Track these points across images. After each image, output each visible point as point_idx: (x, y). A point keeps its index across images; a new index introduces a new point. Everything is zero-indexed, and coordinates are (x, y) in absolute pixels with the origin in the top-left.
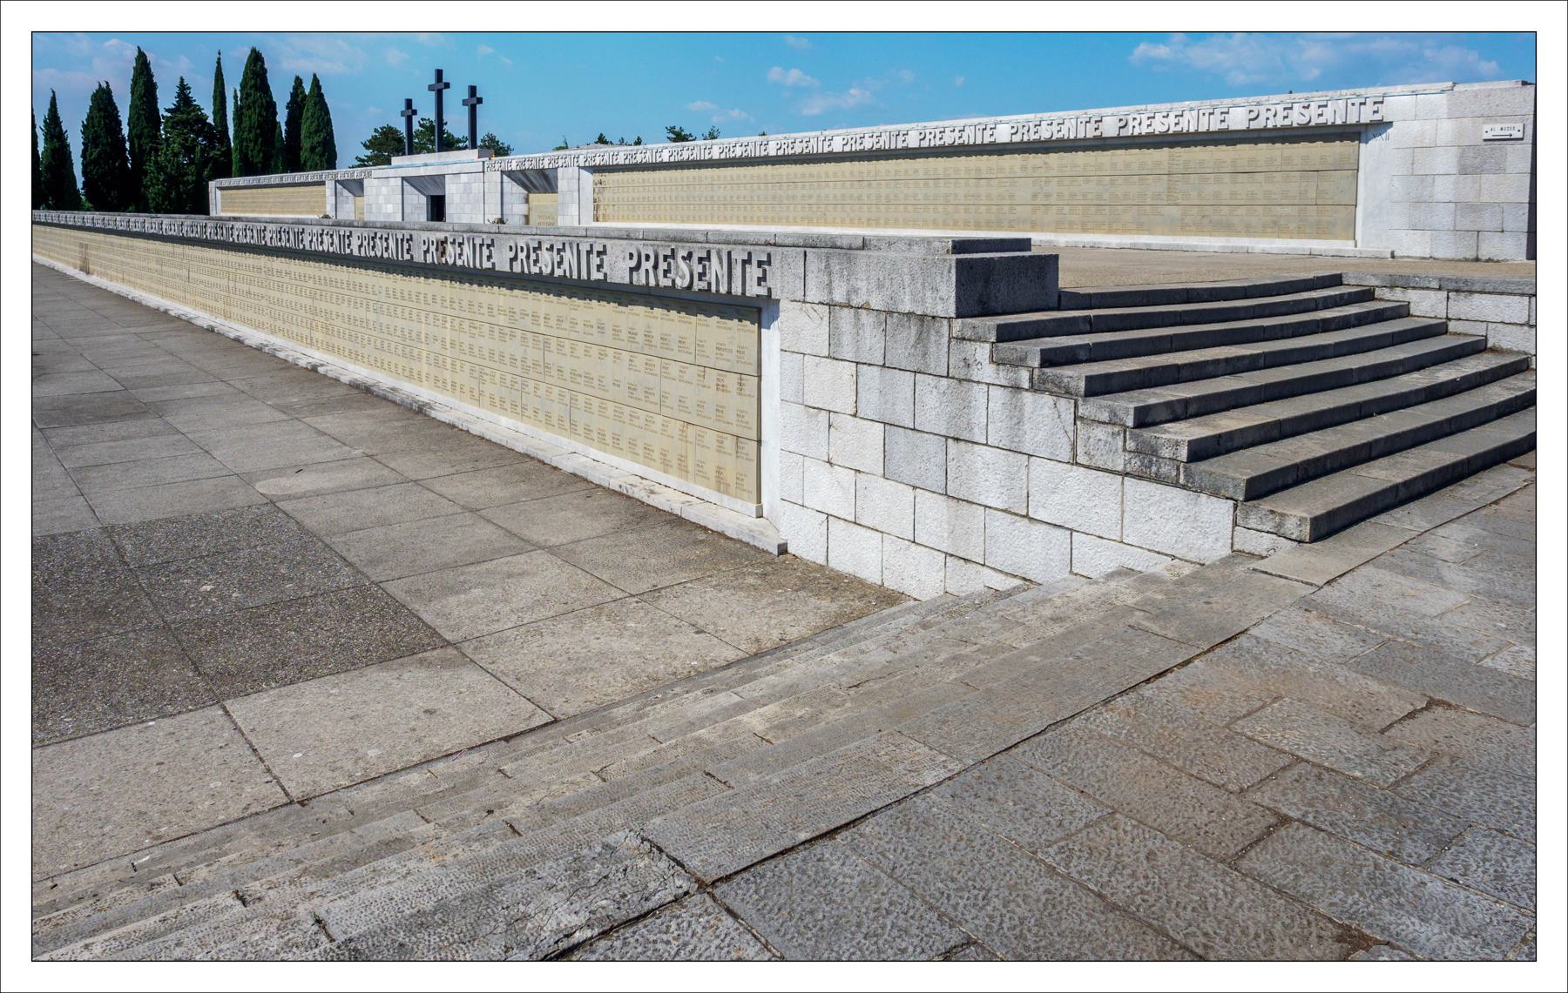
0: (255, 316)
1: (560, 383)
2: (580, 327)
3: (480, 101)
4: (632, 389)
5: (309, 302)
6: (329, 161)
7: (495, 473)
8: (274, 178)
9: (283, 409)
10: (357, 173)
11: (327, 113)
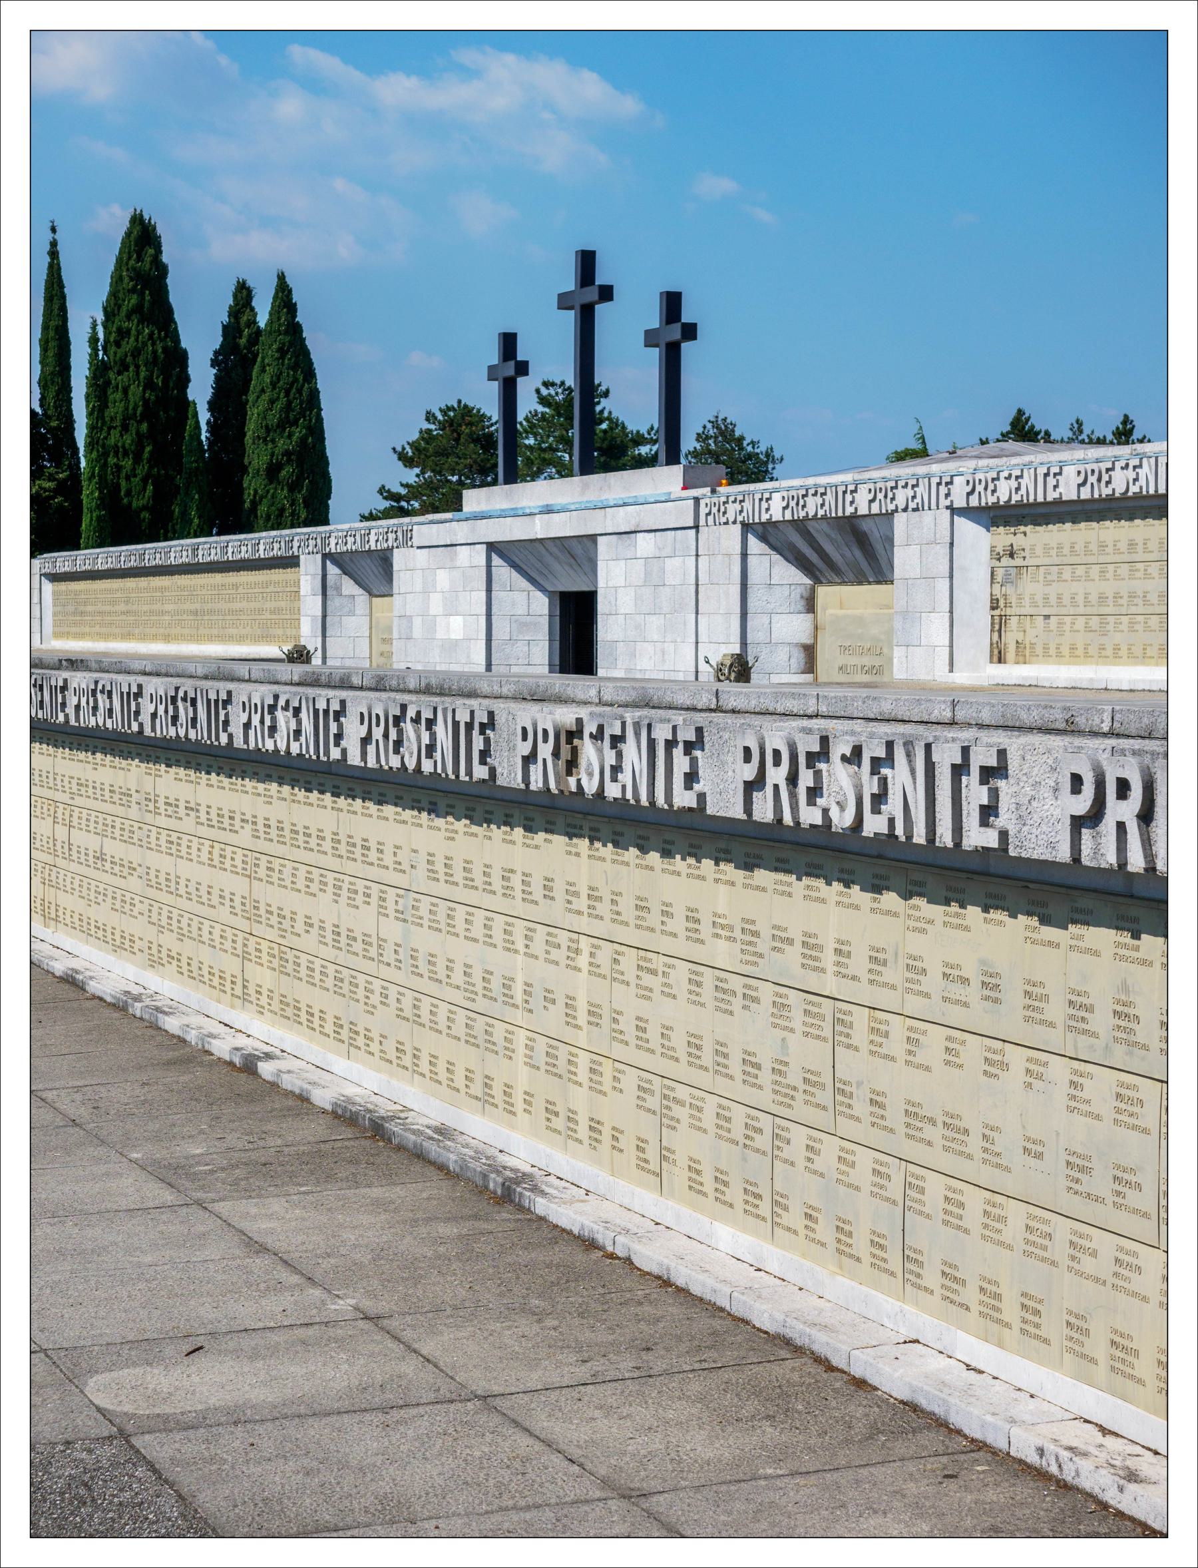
0: (114, 920)
1: (876, 1137)
2: (933, 982)
3: (690, 332)
4: (1078, 1166)
5: (239, 885)
6: (316, 511)
7: (695, 1387)
8: (177, 550)
9: (169, 1173)
10: (377, 535)
11: (310, 374)
